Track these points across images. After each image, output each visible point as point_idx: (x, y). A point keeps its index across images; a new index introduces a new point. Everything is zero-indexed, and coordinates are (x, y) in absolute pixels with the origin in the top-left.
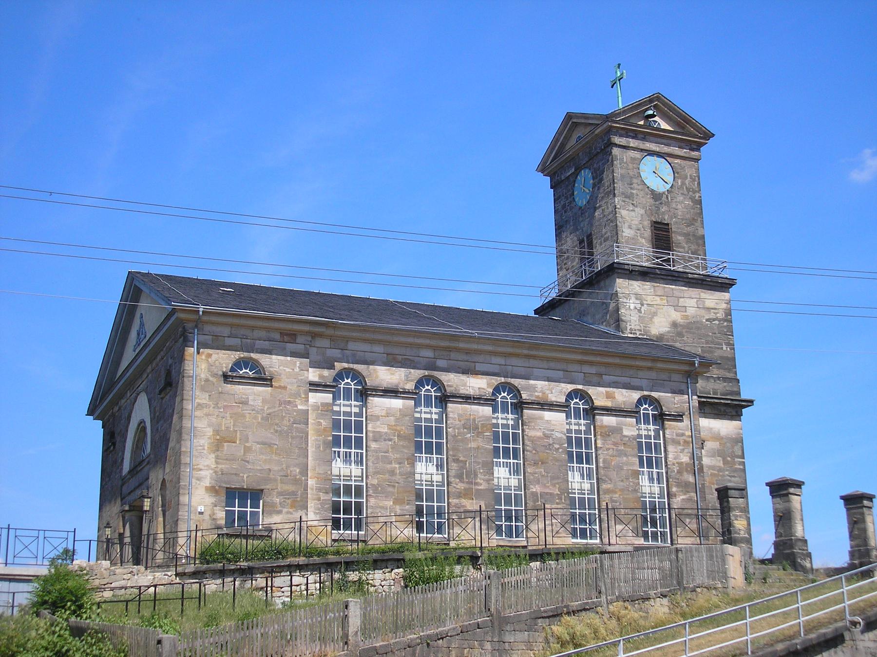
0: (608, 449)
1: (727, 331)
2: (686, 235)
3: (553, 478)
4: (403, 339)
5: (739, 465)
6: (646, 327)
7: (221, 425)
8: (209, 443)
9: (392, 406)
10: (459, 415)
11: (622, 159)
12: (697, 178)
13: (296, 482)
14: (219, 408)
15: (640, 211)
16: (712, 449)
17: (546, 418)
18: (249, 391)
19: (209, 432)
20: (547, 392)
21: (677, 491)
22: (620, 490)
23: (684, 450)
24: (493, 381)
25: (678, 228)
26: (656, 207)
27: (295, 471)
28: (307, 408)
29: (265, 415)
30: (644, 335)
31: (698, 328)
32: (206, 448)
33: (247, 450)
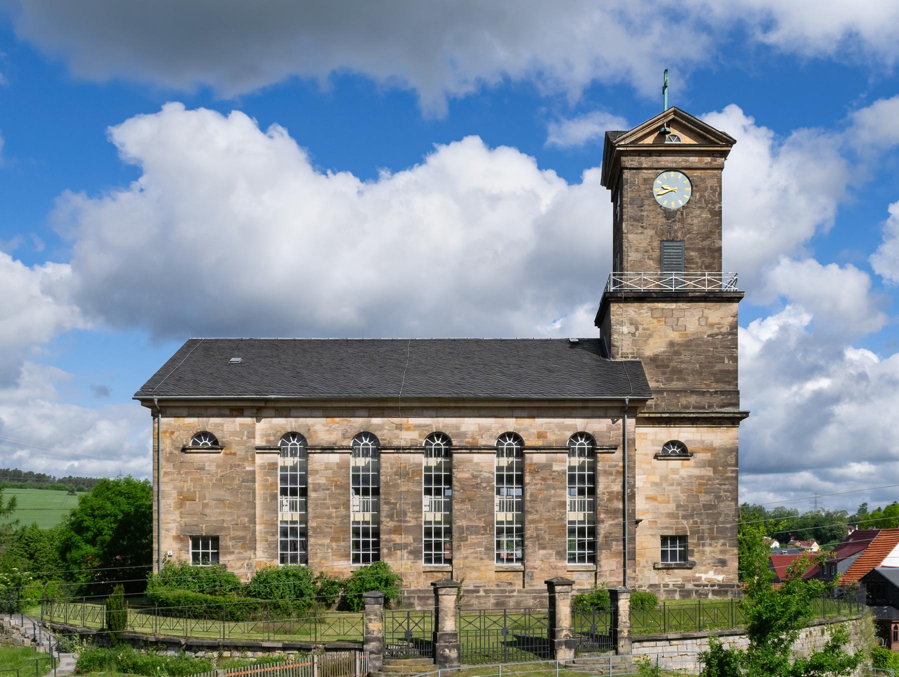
0: (536, 484)
1: (731, 345)
2: (701, 250)
3: (479, 513)
4: (335, 405)
5: (732, 473)
6: (639, 349)
7: (183, 487)
8: (174, 503)
9: (330, 461)
10: (391, 464)
11: (633, 183)
12: (718, 189)
13: (245, 528)
14: (181, 474)
15: (650, 232)
16: (702, 460)
17: (475, 461)
18: (205, 459)
19: (174, 493)
20: (478, 437)
21: (605, 518)
22: (546, 520)
23: (616, 479)
24: (425, 432)
25: (692, 244)
26: (668, 226)
27: (245, 520)
28: (253, 469)
29: (219, 477)
30: (636, 358)
31: (698, 345)
32: (172, 506)
33: (205, 506)
